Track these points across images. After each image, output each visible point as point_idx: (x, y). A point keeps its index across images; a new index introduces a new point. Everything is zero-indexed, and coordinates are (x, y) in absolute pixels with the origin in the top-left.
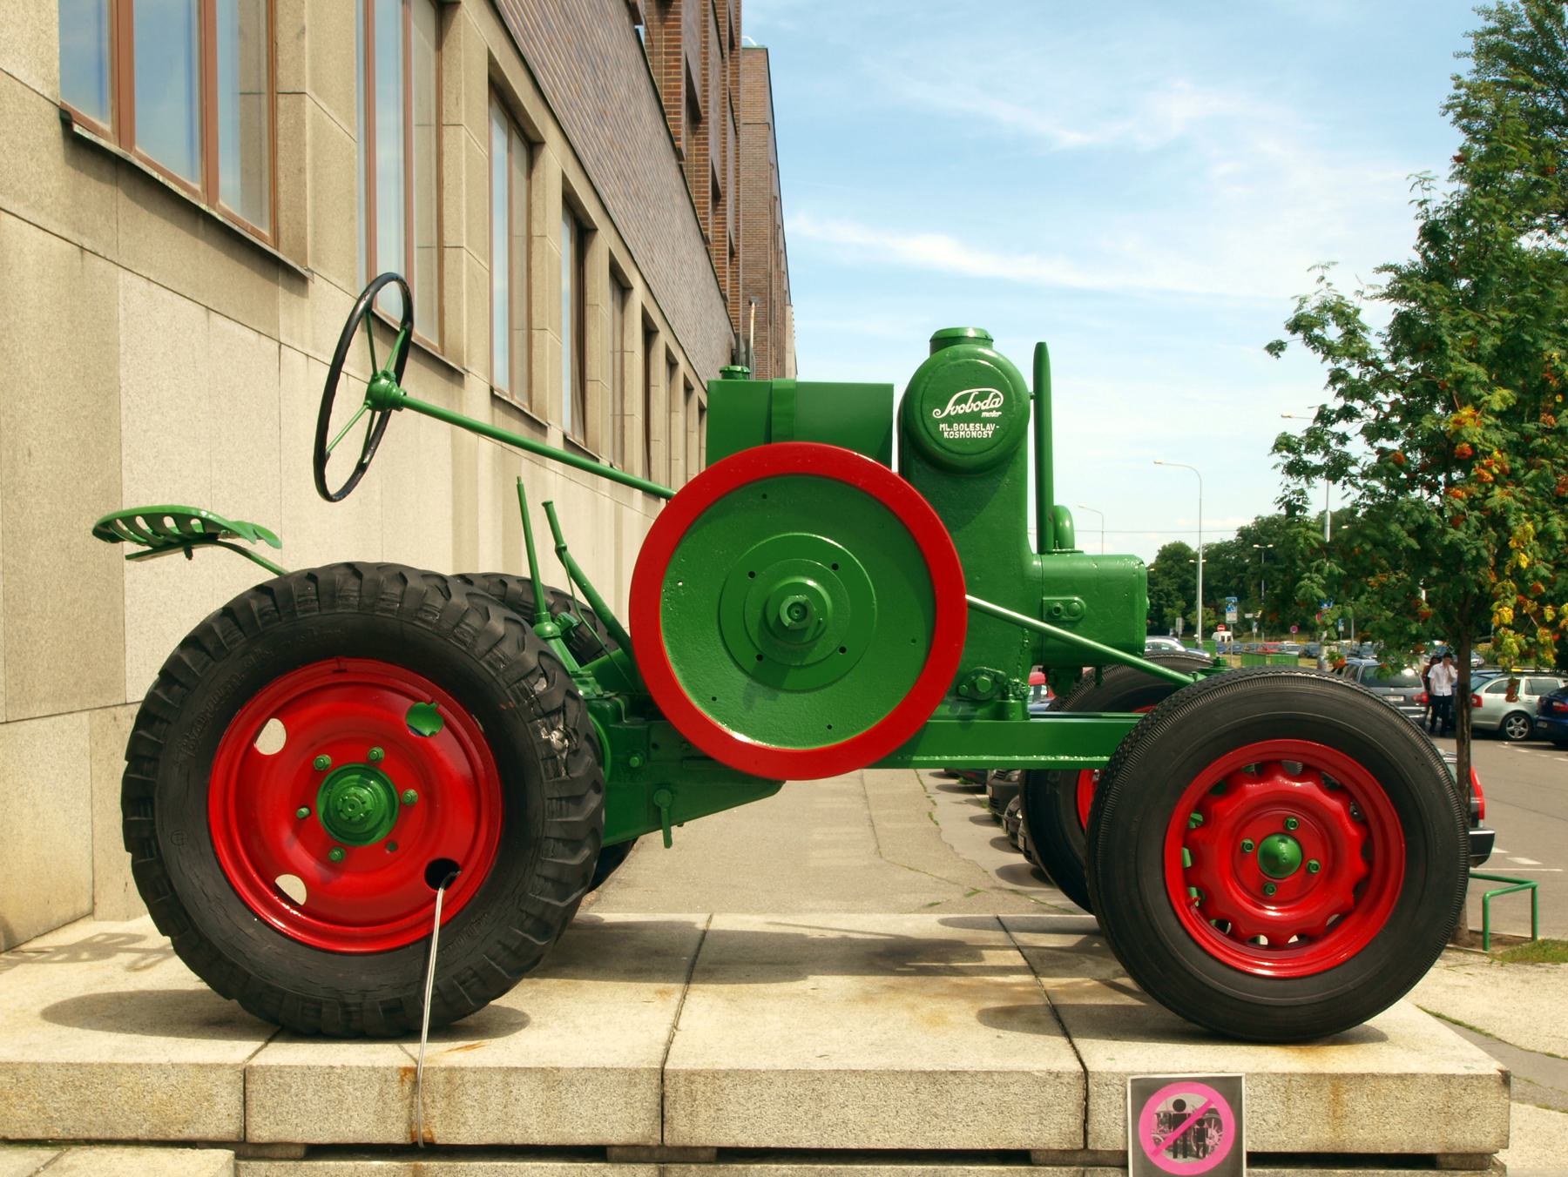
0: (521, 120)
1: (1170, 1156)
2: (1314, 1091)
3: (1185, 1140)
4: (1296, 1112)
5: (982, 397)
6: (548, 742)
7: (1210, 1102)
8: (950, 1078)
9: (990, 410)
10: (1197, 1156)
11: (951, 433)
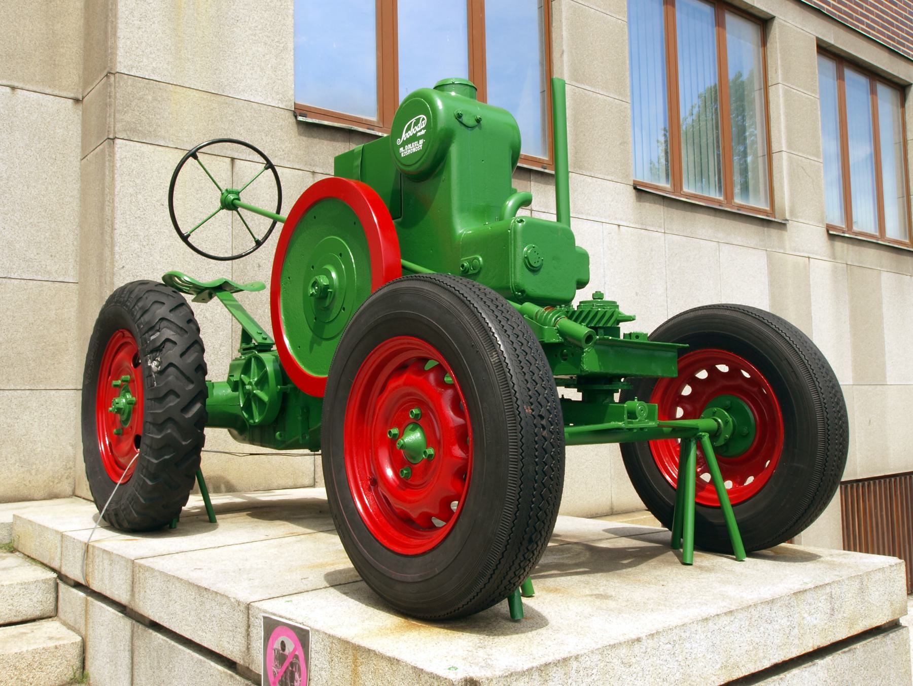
0: (883, 74)
2: (345, 656)
5: (416, 124)
9: (420, 131)
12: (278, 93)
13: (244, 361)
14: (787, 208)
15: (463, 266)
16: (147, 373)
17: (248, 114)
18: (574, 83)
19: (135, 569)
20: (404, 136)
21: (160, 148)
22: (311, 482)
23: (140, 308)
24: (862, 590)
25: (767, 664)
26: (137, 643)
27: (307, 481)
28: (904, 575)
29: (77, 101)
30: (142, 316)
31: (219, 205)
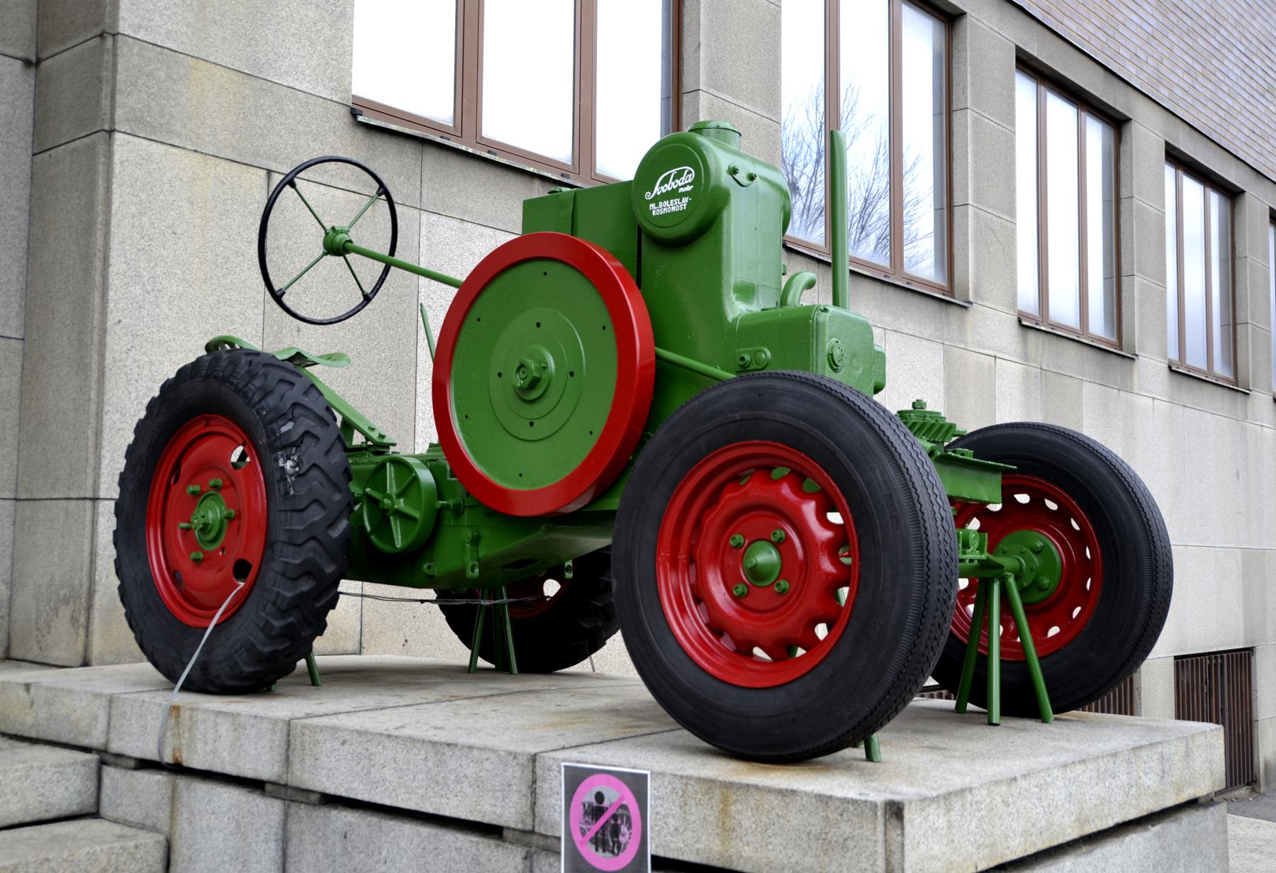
0: (1094, 103)
1: (592, 848)
2: (707, 797)
3: (603, 834)
4: (692, 818)
5: (679, 175)
6: (283, 468)
7: (622, 798)
8: (447, 749)
9: (685, 186)
10: (613, 852)
11: (657, 210)
12: (331, 80)
13: (373, 466)
14: (971, 286)
15: (743, 359)
16: (277, 475)
17: (292, 107)
18: (711, 91)
19: (289, 734)
20: (656, 189)
21: (174, 150)
22: (357, 647)
23: (258, 389)
24: (1188, 754)
25: (1110, 823)
26: (294, 828)
27: (351, 645)
28: (1222, 742)
29: (27, 63)
30: (263, 398)
31: (321, 250)
